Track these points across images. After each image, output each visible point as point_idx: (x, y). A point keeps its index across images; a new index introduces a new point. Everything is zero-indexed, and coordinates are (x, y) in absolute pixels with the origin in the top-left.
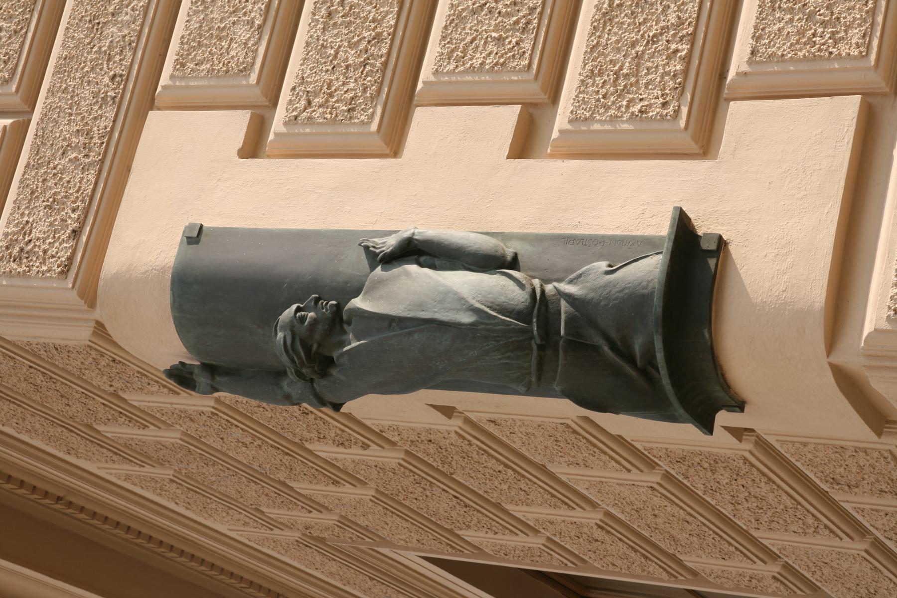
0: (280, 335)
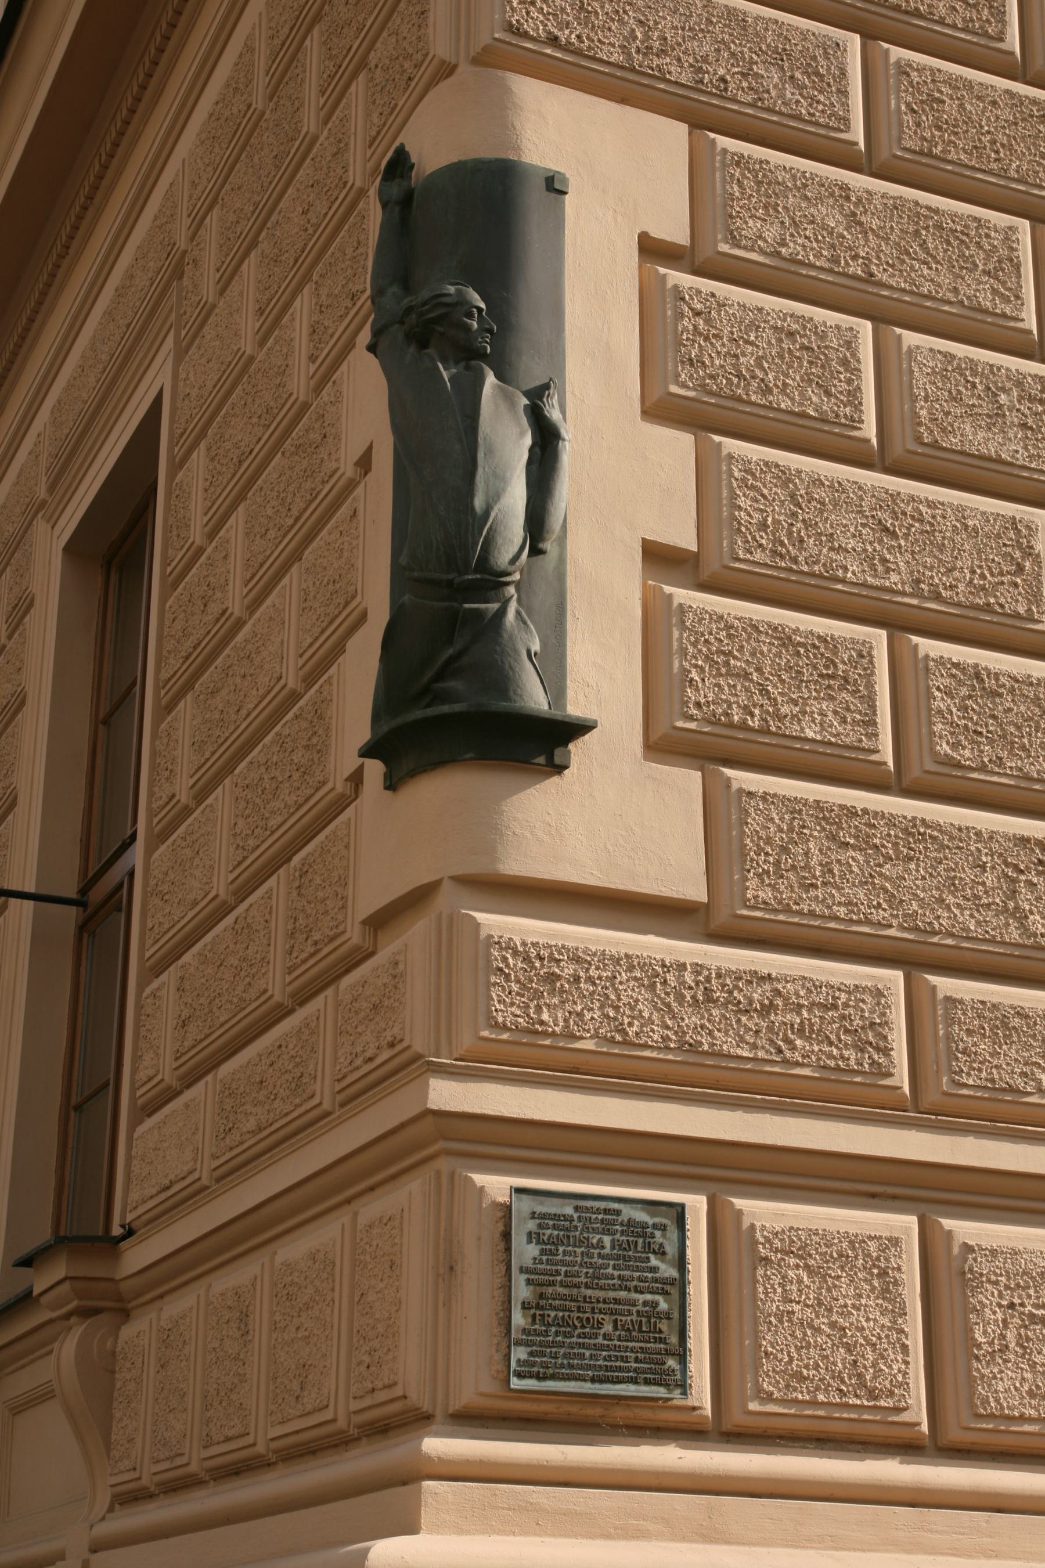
0: (452, 289)
